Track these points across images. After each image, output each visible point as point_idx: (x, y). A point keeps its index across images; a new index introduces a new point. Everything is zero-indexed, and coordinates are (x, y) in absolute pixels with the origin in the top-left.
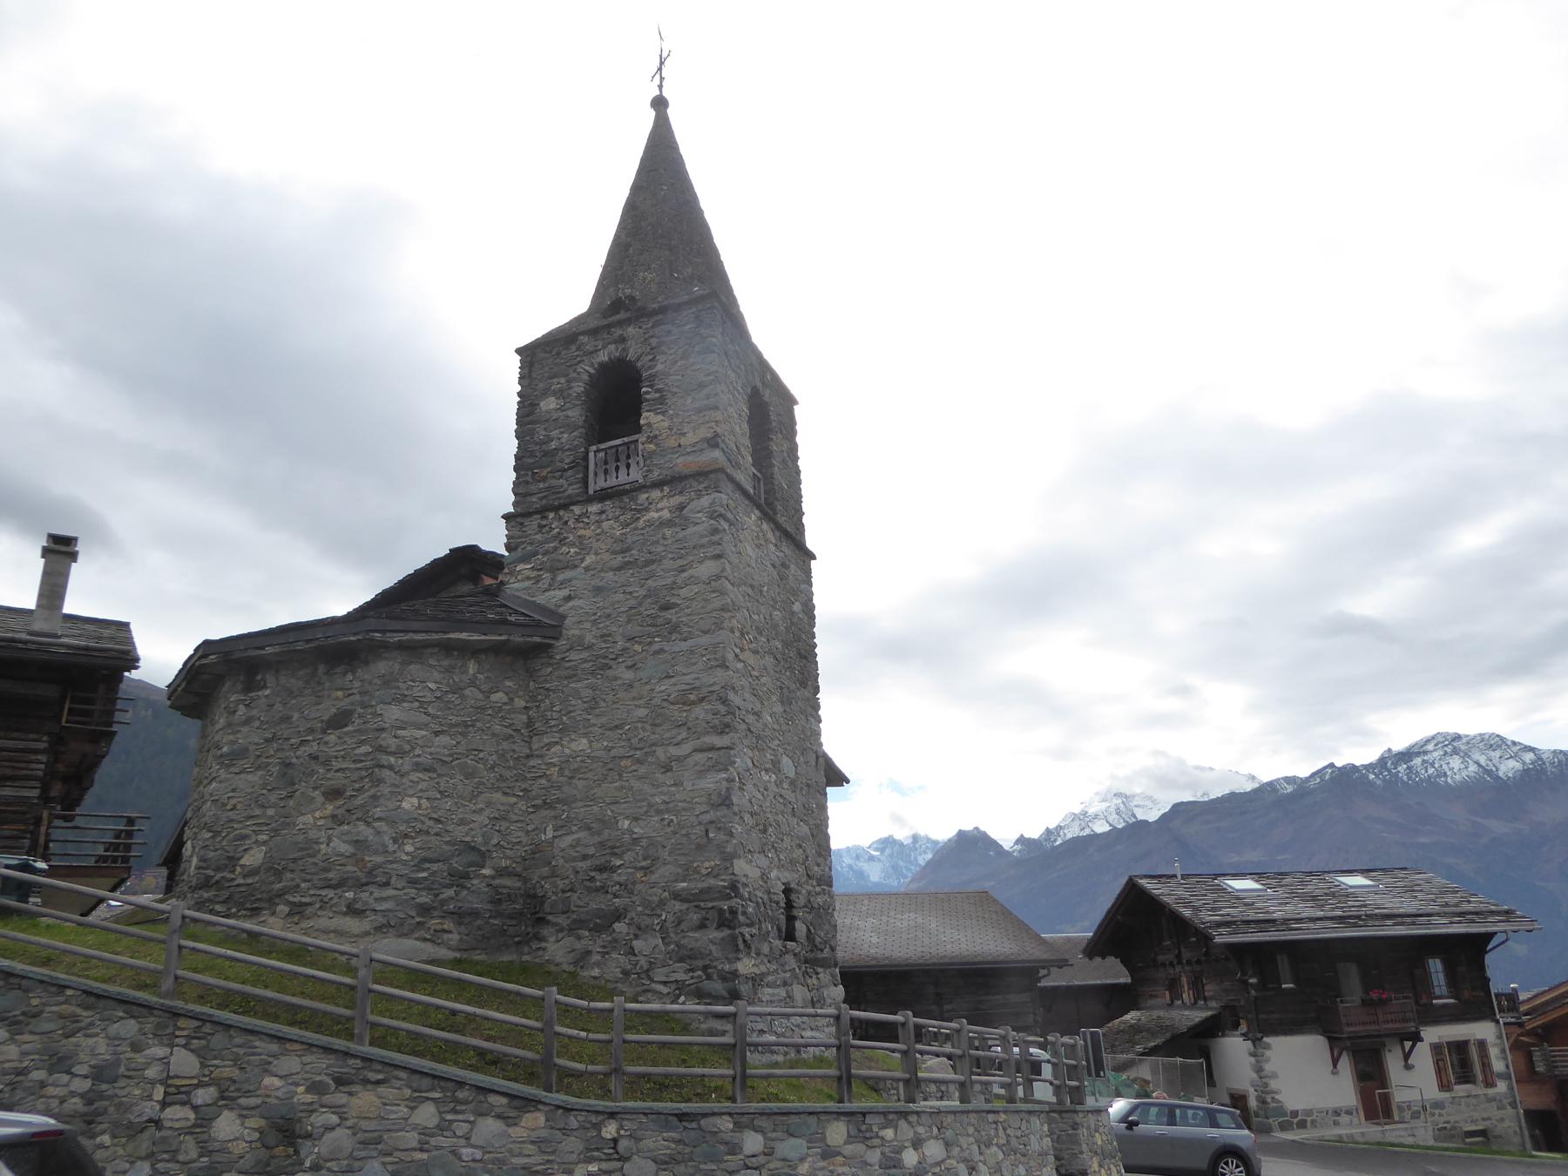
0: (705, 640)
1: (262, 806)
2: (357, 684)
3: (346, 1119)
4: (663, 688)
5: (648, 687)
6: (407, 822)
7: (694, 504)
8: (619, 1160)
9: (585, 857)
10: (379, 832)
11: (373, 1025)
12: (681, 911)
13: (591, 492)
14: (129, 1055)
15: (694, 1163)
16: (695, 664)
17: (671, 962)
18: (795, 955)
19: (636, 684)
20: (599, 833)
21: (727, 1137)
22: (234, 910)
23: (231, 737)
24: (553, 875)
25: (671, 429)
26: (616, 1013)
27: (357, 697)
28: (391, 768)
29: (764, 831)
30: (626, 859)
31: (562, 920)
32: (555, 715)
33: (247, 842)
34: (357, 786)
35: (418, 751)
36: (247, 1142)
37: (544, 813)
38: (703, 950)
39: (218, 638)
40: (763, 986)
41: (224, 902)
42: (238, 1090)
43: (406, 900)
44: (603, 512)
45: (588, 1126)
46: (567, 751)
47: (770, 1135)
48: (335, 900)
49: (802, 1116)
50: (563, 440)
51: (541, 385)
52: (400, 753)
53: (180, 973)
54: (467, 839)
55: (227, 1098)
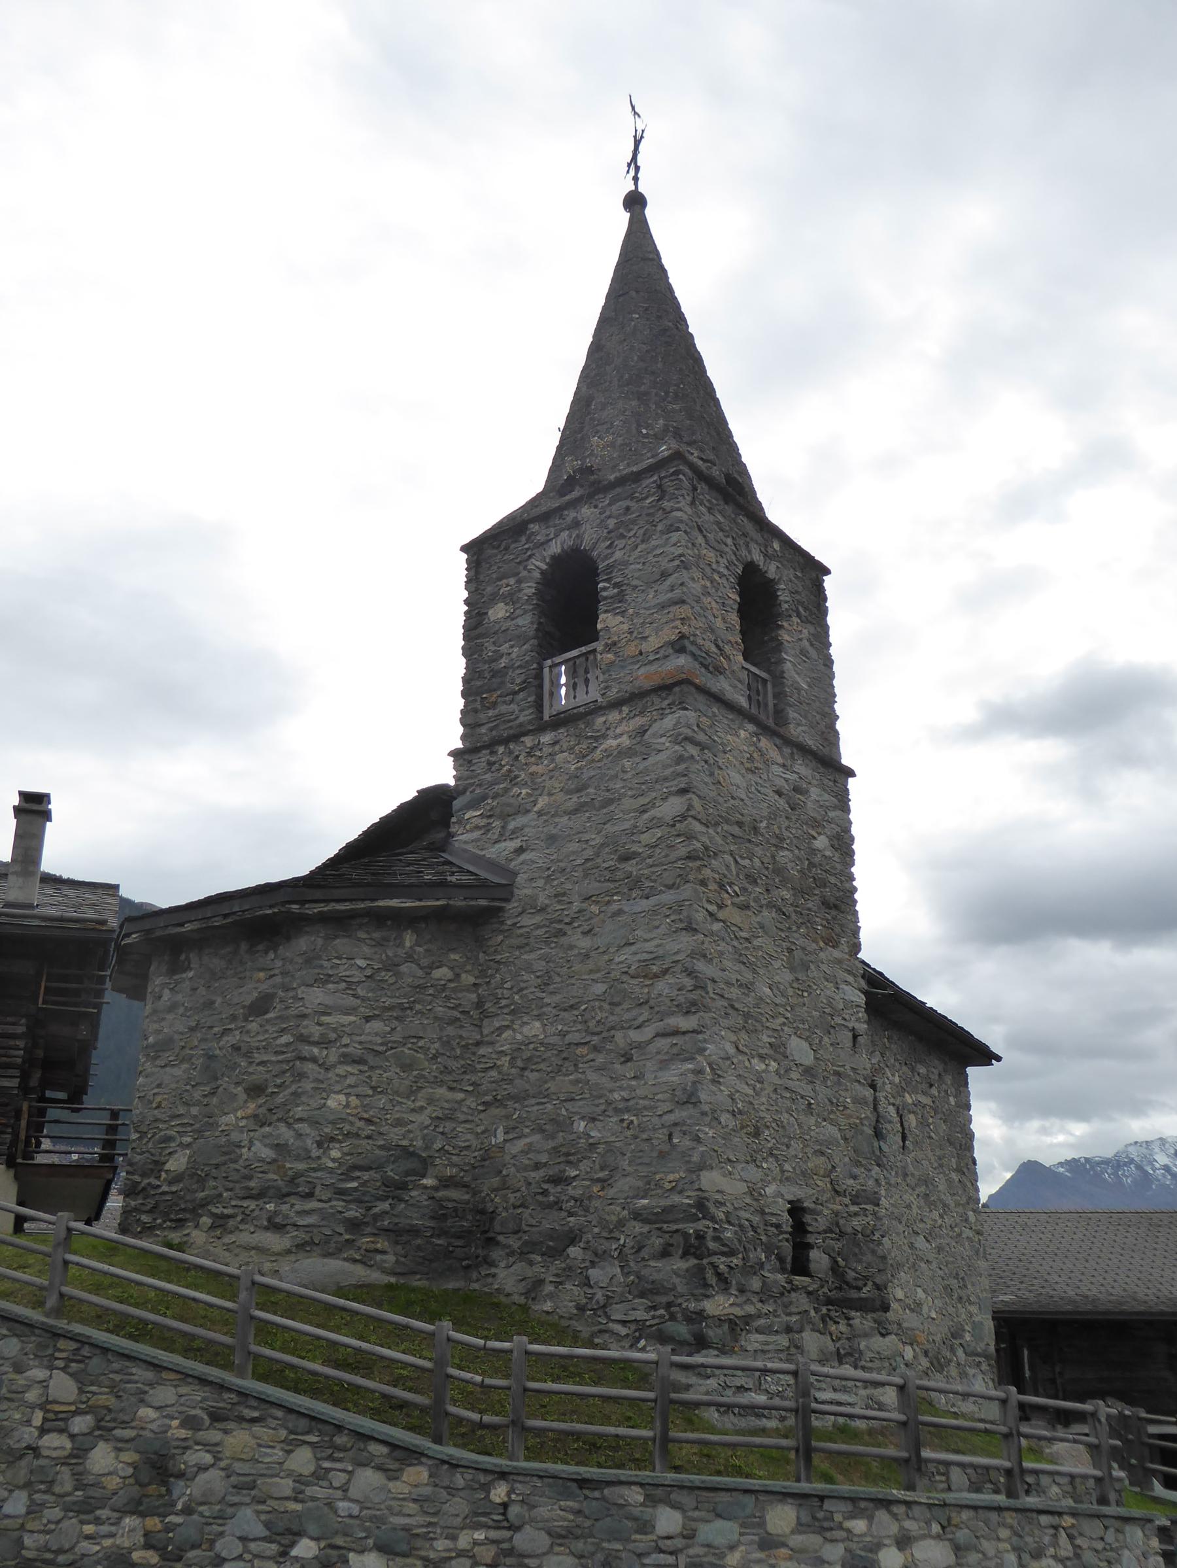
0: (669, 897)
1: (186, 1104)
2: (279, 963)
3: (220, 1459)
4: (623, 958)
5: (606, 957)
6: (333, 1123)
7: (656, 727)
8: (509, 1528)
9: (537, 1166)
10: (301, 1135)
11: (257, 1356)
12: (641, 1234)
13: (546, 717)
14: (11, 1376)
15: (593, 1540)
16: (657, 927)
17: (630, 1297)
18: (809, 1293)
19: (593, 954)
20: (553, 1138)
21: (636, 1511)
22: (159, 1221)
23: (156, 1026)
24: (504, 1186)
25: (631, 633)
26: (515, 1354)
27: (278, 979)
28: (314, 1060)
29: (757, 1134)
30: (582, 1168)
31: (514, 1243)
32: (507, 993)
33: (173, 1144)
34: (279, 1081)
35: (346, 1040)
36: (121, 1478)
37: (495, 1111)
38: (665, 1283)
39: (183, 903)
40: (749, 1332)
41: (150, 1211)
42: (114, 1420)
43: (333, 1214)
44: (556, 743)
45: (477, 1486)
46: (519, 1037)
47: (690, 1514)
48: (257, 1213)
49: (734, 1494)
50: (514, 656)
51: (489, 589)
52: (324, 1043)
53: (65, 1289)
54: (405, 1143)
55: (102, 1430)
